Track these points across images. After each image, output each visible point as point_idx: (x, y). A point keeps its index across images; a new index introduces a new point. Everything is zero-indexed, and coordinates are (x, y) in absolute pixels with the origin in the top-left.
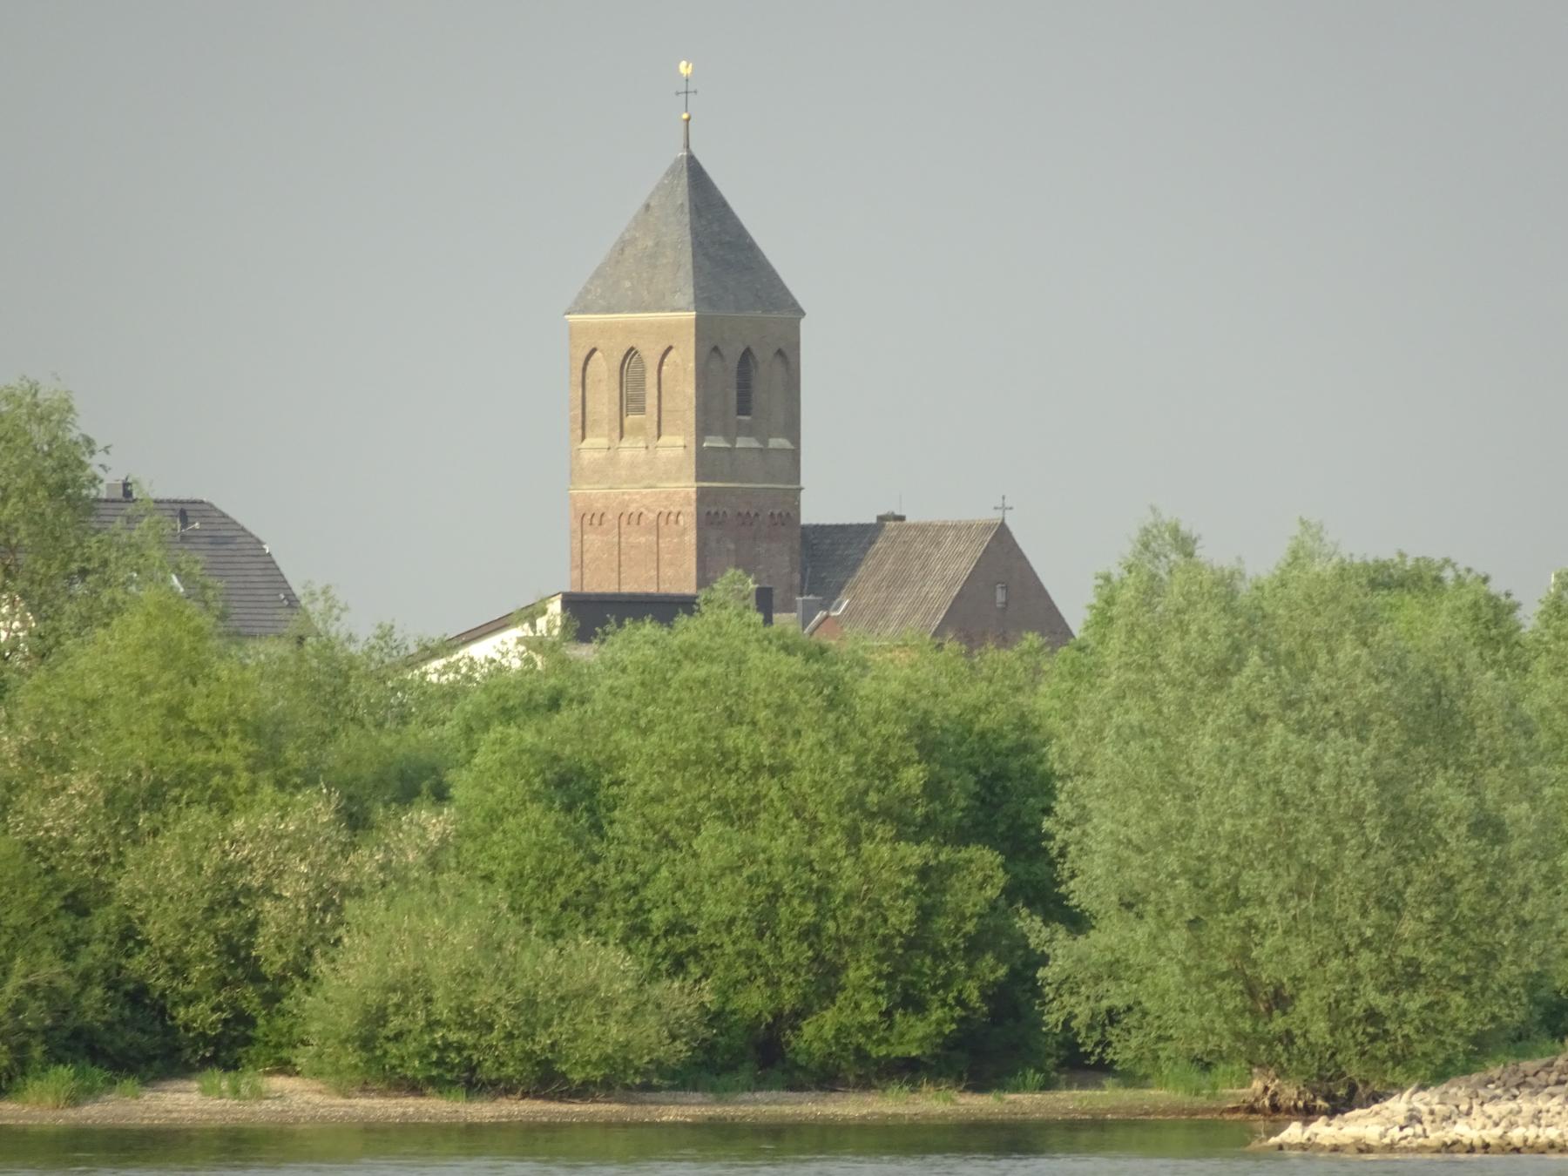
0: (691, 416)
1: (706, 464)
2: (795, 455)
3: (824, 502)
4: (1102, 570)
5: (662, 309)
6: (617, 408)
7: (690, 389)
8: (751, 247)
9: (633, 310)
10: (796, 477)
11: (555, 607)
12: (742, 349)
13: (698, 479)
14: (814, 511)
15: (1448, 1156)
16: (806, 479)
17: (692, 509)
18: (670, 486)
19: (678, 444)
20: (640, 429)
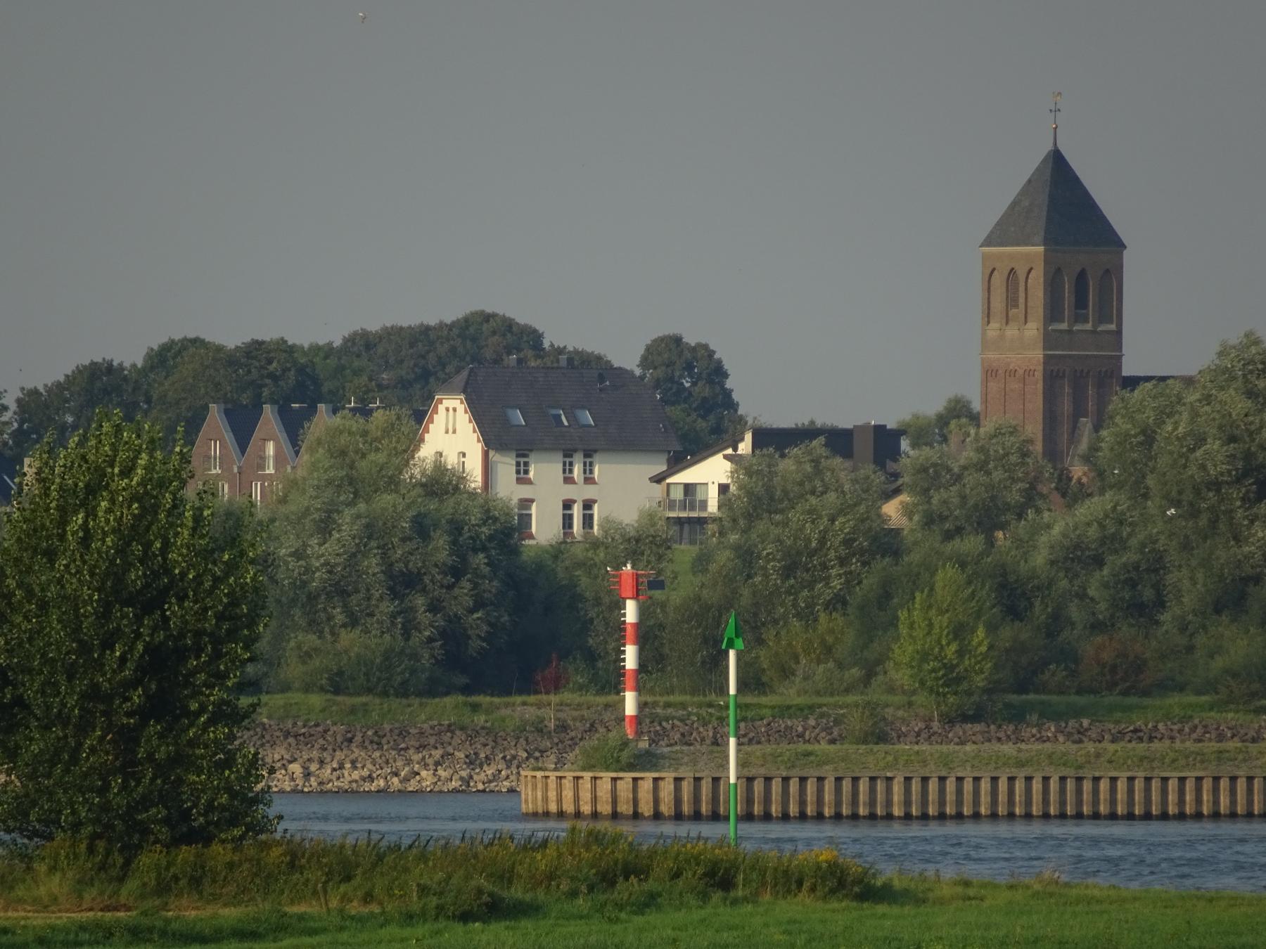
0: (1041, 311)
1: (1049, 340)
2: (1119, 333)
4: (440, 450)
5: (1027, 245)
6: (1004, 305)
7: (1040, 294)
8: (1104, 217)
9: (1012, 245)
10: (1119, 345)
11: (748, 437)
12: (1079, 269)
13: (1045, 348)
15: (1141, 748)
16: (1126, 349)
17: (1041, 368)
19: (1033, 330)
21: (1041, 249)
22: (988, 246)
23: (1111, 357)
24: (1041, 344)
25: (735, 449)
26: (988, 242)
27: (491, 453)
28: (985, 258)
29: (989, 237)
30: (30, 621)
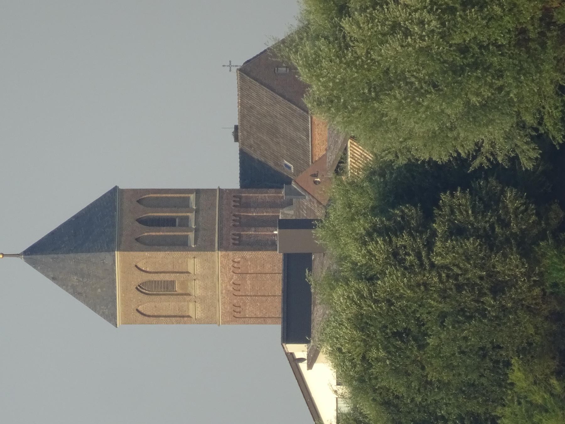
1: (205, 246)
2: (198, 192)
3: (226, 175)
11: (291, 348)
13: (214, 251)
14: (231, 180)
18: (218, 265)
19: (194, 262)
20: (184, 284)
21: (117, 253)
22: (116, 318)
23: (221, 198)
24: (209, 253)
25: (302, 360)
26: (111, 318)
27: (284, 344)
28: (127, 321)
29: (103, 315)
30: (424, 40)
